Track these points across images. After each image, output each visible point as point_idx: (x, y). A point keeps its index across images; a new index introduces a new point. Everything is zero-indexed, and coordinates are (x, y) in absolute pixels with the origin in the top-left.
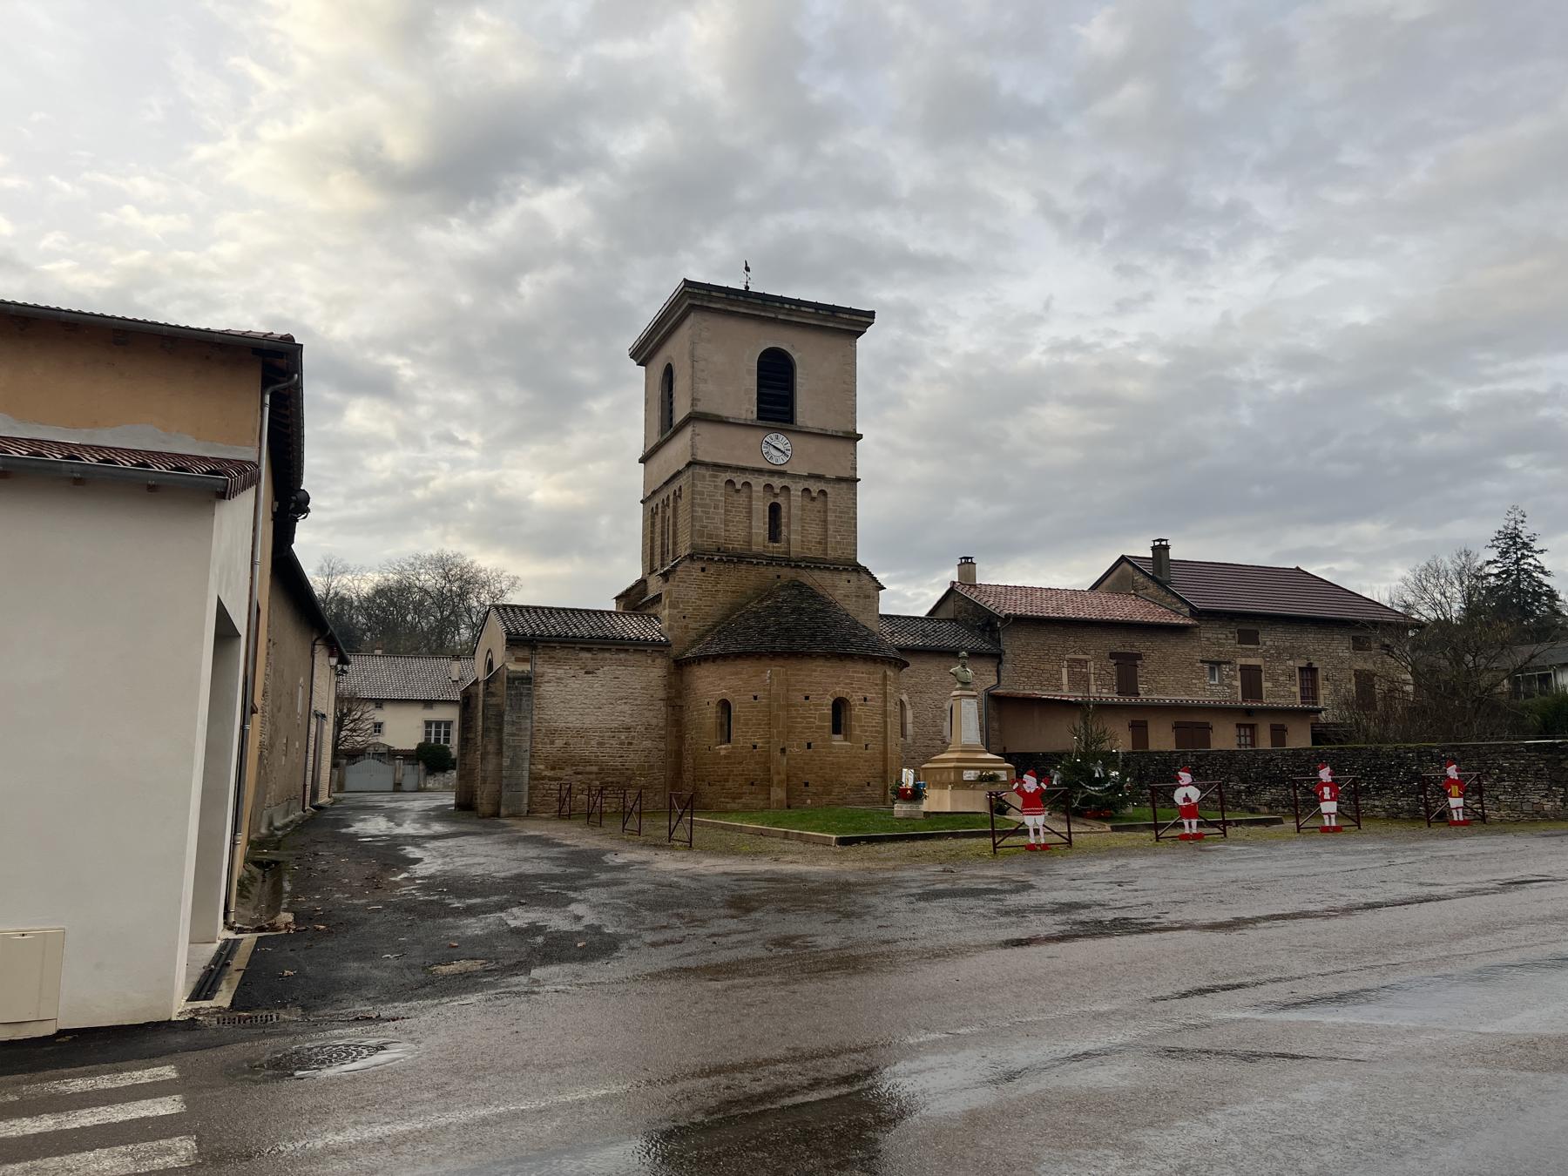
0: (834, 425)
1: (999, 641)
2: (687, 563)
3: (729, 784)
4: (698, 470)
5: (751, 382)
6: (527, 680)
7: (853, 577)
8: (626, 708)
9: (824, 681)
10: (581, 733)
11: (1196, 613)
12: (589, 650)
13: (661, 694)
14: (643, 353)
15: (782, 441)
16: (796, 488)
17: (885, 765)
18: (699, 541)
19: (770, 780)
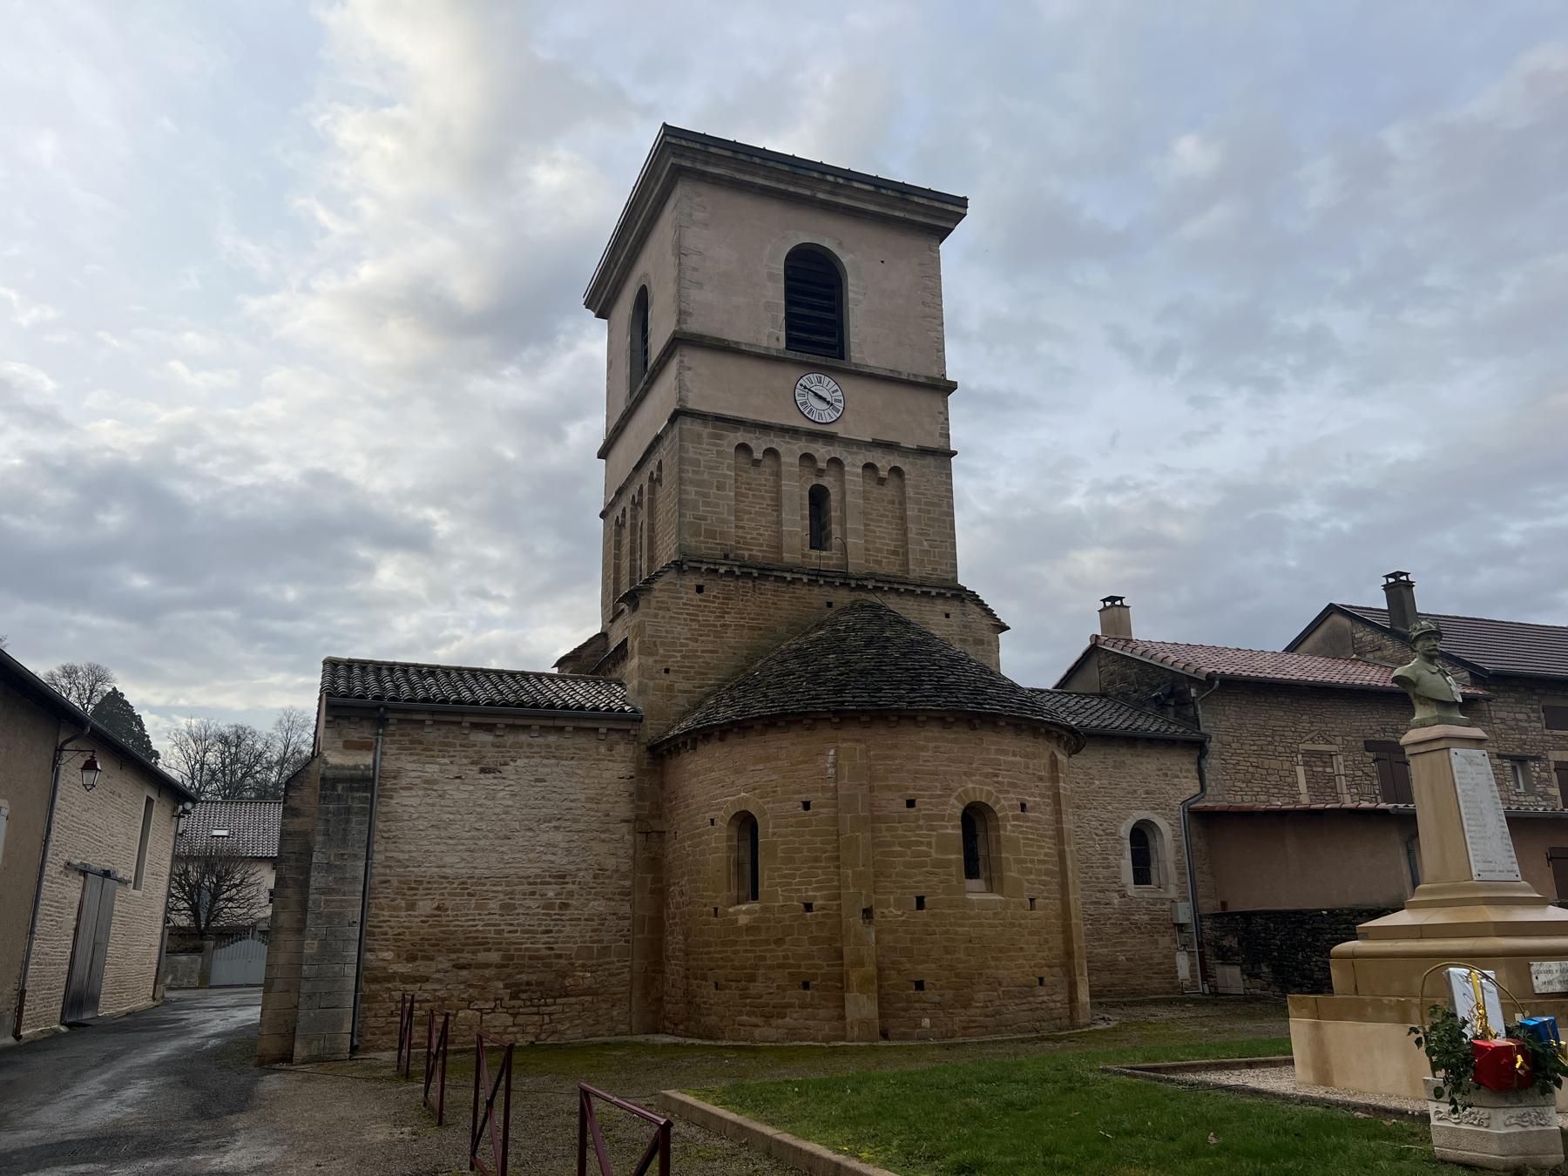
1: (1196, 721)
2: (670, 576)
3: (756, 988)
4: (687, 424)
5: (776, 293)
6: (365, 783)
7: (954, 608)
8: (558, 837)
9: (946, 769)
10: (466, 887)
11: (1478, 676)
12: (490, 728)
13: (624, 809)
14: (601, 300)
15: (827, 386)
16: (854, 463)
18: (692, 541)
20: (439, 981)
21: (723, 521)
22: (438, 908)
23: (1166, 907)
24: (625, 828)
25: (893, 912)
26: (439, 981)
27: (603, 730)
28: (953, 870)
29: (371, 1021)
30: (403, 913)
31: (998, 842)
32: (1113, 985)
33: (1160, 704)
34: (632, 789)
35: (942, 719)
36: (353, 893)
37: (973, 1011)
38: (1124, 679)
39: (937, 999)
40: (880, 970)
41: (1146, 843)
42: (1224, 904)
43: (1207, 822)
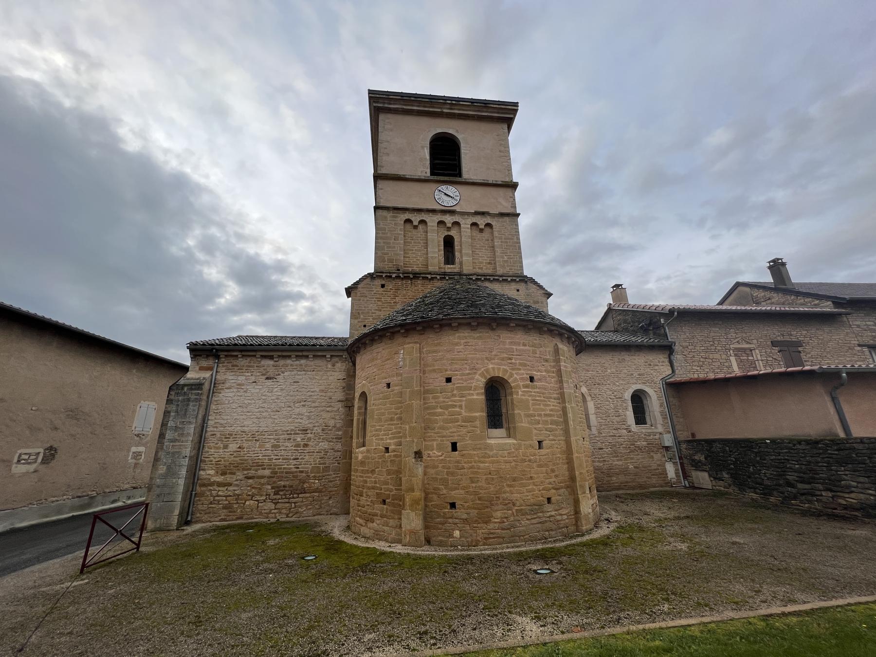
0: (499, 178)
7: (522, 286)
8: (304, 410)
12: (271, 358)
15: (451, 190)
16: (466, 223)
17: (571, 469)
19: (401, 498)
20: (237, 485)
21: (397, 255)
22: (239, 447)
23: (657, 437)
24: (340, 405)
25: (436, 453)
26: (237, 485)
27: (328, 356)
28: (478, 423)
29: (200, 507)
30: (221, 450)
31: (512, 403)
32: (627, 482)
33: (645, 330)
34: (344, 385)
35: (469, 324)
36: (187, 441)
37: (491, 526)
38: (625, 321)
39: (465, 516)
40: (427, 494)
41: (642, 402)
42: (693, 435)
43: (677, 389)
